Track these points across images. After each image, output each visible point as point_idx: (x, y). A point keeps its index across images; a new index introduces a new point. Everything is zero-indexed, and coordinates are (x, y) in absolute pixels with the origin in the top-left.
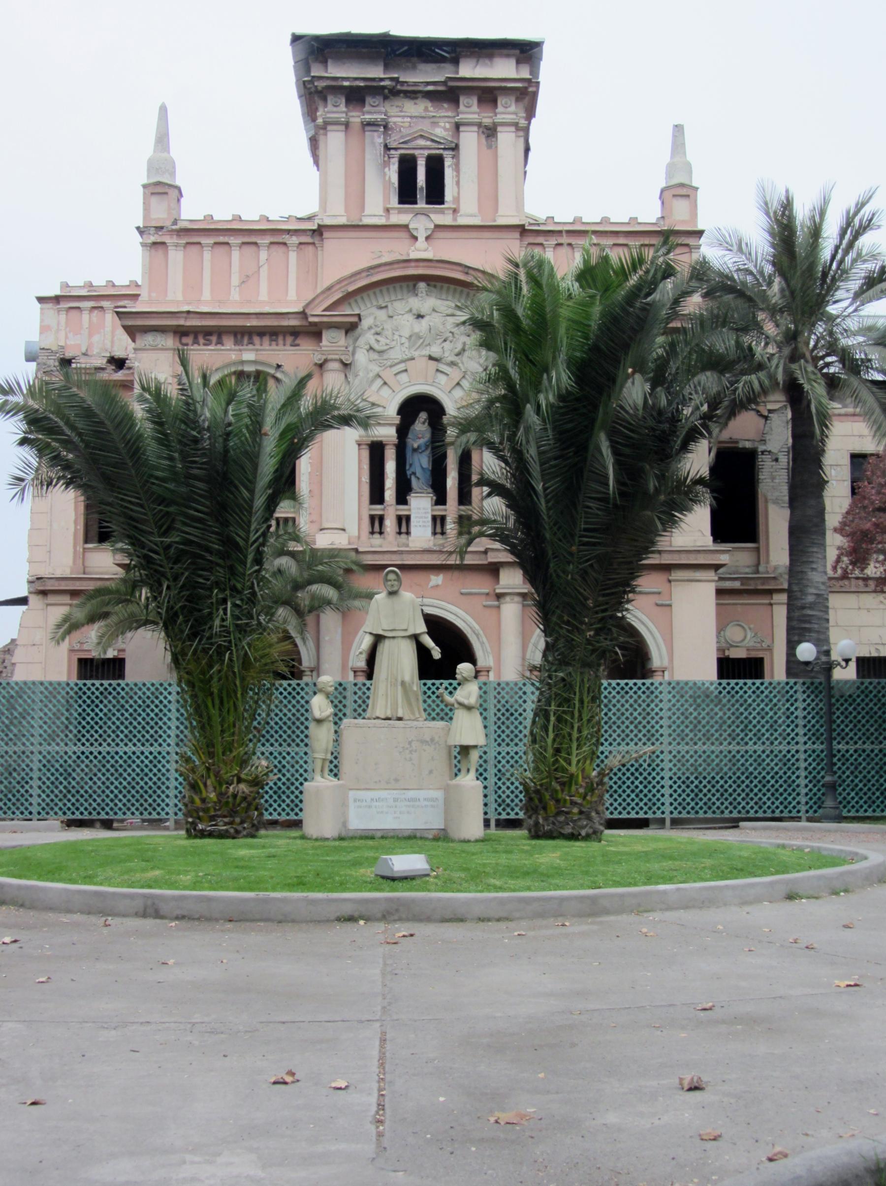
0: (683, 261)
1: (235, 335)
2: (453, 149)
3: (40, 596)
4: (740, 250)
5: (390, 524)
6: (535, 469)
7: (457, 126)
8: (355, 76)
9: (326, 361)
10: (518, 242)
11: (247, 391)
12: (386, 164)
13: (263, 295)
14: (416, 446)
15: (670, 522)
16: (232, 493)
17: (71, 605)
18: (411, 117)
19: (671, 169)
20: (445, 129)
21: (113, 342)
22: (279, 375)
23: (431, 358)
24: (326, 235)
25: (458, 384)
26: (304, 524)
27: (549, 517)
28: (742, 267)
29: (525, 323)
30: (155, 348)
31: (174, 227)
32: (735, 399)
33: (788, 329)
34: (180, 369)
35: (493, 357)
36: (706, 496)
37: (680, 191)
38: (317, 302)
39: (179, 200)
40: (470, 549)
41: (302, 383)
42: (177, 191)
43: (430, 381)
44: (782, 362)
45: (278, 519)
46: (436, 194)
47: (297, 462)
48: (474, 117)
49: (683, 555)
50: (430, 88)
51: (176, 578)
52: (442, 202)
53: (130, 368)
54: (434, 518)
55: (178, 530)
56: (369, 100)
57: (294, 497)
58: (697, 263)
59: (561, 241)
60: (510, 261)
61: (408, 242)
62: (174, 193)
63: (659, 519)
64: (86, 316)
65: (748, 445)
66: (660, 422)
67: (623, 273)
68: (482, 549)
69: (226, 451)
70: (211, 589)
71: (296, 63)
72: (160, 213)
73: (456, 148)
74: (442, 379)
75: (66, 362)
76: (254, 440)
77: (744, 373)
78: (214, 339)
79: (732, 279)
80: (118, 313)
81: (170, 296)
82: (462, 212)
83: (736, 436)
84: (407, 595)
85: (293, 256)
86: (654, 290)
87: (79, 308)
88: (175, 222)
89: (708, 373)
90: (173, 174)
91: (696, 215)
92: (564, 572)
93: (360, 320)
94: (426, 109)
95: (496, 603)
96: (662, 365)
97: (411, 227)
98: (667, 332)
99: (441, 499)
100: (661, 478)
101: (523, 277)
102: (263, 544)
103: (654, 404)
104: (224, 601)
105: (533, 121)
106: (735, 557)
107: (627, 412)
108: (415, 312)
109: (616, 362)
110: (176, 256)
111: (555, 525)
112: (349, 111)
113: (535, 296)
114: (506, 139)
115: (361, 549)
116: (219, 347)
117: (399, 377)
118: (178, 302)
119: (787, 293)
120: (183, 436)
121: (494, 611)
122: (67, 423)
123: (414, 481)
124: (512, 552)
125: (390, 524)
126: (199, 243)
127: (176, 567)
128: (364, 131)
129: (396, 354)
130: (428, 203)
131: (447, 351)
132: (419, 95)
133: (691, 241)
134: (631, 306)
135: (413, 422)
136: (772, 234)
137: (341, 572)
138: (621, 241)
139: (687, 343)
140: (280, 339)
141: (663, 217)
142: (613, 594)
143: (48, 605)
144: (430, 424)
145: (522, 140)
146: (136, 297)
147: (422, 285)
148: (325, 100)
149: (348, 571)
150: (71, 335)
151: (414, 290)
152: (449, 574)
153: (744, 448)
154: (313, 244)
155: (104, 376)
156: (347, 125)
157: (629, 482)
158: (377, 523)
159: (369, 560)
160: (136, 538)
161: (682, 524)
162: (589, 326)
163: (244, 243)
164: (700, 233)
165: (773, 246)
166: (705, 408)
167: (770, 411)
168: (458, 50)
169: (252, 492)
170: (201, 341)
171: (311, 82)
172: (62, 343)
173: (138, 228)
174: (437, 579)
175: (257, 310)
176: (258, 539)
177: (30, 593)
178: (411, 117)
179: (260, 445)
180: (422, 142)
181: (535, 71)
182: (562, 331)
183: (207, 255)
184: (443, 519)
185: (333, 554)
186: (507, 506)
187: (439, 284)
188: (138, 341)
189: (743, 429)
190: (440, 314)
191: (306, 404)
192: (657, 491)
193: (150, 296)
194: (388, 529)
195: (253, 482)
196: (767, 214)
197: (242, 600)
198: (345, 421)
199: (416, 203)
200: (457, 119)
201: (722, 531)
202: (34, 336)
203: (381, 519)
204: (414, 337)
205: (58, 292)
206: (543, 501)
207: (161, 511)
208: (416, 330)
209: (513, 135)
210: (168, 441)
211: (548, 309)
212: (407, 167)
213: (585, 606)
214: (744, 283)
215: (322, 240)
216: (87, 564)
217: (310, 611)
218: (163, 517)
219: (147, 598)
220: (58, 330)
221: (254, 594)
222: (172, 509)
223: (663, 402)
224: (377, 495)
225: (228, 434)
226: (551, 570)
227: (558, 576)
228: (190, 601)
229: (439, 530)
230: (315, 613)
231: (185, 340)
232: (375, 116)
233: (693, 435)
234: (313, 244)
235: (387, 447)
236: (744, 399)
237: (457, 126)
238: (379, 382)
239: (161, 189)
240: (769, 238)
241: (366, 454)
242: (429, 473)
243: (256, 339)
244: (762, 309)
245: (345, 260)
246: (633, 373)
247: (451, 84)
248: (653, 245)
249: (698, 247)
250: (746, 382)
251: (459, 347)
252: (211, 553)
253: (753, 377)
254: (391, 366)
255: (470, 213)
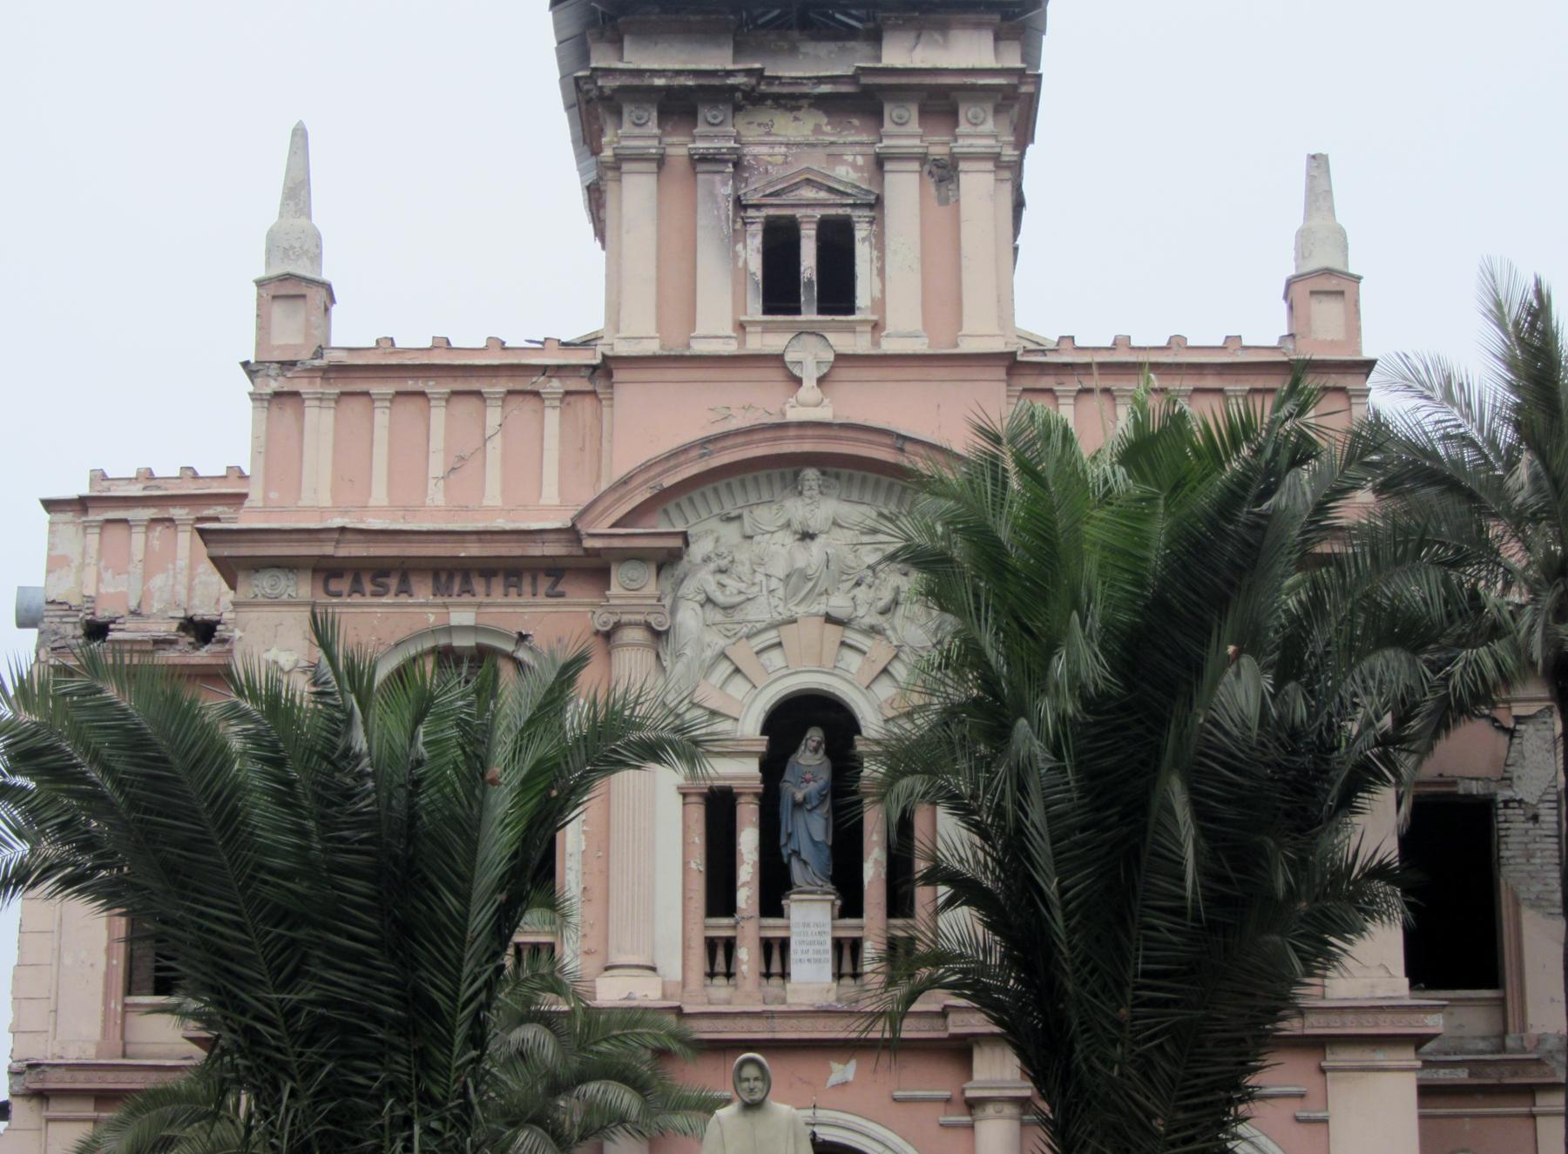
0: (1330, 423)
1: (436, 574)
2: (870, 206)
3: (34, 1103)
4: (1448, 396)
5: (747, 956)
6: (1042, 849)
7: (880, 162)
8: (677, 67)
9: (618, 626)
10: (1003, 386)
11: (456, 695)
12: (738, 236)
13: (493, 495)
14: (799, 796)
15: (1319, 957)
16: (424, 902)
17: (95, 1121)
18: (787, 145)
19: (1304, 240)
20: (854, 166)
21: (190, 589)
22: (522, 655)
23: (829, 619)
24: (619, 375)
25: (885, 671)
26: (572, 956)
27: (1072, 949)
28: (1453, 431)
29: (1015, 557)
30: (274, 602)
31: (317, 363)
32: (1447, 696)
33: (1550, 555)
34: (319, 653)
35: (951, 622)
36: (1393, 899)
37: (1324, 284)
38: (600, 508)
39: (327, 310)
40: (915, 1007)
41: (569, 672)
42: (323, 292)
43: (828, 665)
44: (1540, 621)
45: (518, 947)
46: (837, 292)
47: (559, 835)
48: (912, 144)
49: (1349, 1018)
50: (825, 88)
51: (309, 1072)
52: (851, 310)
53: (224, 641)
54: (838, 944)
55: (314, 977)
56: (705, 113)
57: (551, 902)
58: (1361, 425)
59: (1088, 384)
60: (983, 431)
61: (781, 388)
62: (317, 296)
63: (1297, 949)
64: (138, 537)
65: (1476, 788)
66: (1294, 752)
67: (1213, 455)
68: (937, 1007)
69: (413, 817)
70: (379, 1098)
71: (560, 43)
72: (290, 335)
73: (877, 204)
74: (853, 661)
75: (96, 630)
76: (470, 794)
77: (1463, 643)
78: (393, 582)
79: (1434, 455)
80: (202, 532)
81: (306, 500)
82: (890, 329)
83: (1450, 770)
84: (781, 1110)
85: (552, 417)
86: (1277, 484)
87: (125, 521)
88: (319, 352)
89: (1390, 653)
90: (316, 258)
91: (1359, 329)
92: (1104, 1061)
93: (687, 544)
94: (817, 129)
95: (967, 1119)
96: (1300, 626)
97: (788, 358)
98: (1308, 561)
99: (851, 905)
100: (1300, 865)
101: (1010, 464)
102: (487, 1006)
103: (1281, 716)
104: (407, 1122)
105: (1030, 149)
106: (1455, 1019)
107: (1227, 734)
108: (796, 526)
109: (1203, 633)
110: (320, 421)
111: (1084, 963)
112: (665, 134)
113: (1035, 501)
114: (976, 184)
115: (687, 1009)
116: (403, 599)
117: (765, 656)
118: (322, 511)
119: (1546, 484)
120: (325, 787)
121: (962, 1135)
122: (95, 758)
123: (796, 870)
124: (998, 1022)
125: (747, 956)
126: (367, 394)
127: (309, 1051)
128: (696, 173)
129: (759, 612)
130: (821, 311)
131: (863, 604)
132: (804, 102)
133: (1351, 382)
134: (1230, 522)
135: (794, 749)
136: (1511, 365)
137: (648, 1055)
138: (1210, 382)
139: (1345, 593)
140: (527, 587)
141: (1292, 335)
142: (1205, 1105)
143: (49, 1120)
144: (828, 753)
145: (1007, 188)
146: (239, 498)
147: (811, 474)
148: (618, 113)
149: (662, 1054)
150: (108, 576)
151: (794, 485)
152: (870, 1061)
153: (1469, 796)
154: (594, 393)
155: (171, 656)
156: (661, 161)
157: (1233, 875)
158: (720, 954)
159: (705, 1030)
160: (229, 993)
161: (1346, 960)
162: (1146, 559)
163: (455, 393)
164: (1369, 365)
165: (1514, 389)
166: (1387, 720)
167: (1519, 719)
168: (880, 15)
169: (465, 898)
170: (368, 587)
171: (591, 78)
172: (90, 591)
173: (245, 364)
174: (843, 1071)
175: (480, 526)
176: (476, 994)
177: (13, 1095)
178: (787, 145)
179: (481, 804)
180: (809, 194)
181: (1031, 53)
182: (1091, 566)
183: (382, 417)
184: (856, 945)
185: (632, 1018)
186: (988, 926)
187: (845, 472)
188: (241, 588)
189: (1465, 755)
190: (842, 534)
191: (577, 714)
192: (1292, 895)
193: (266, 497)
194: (744, 968)
195: (467, 880)
196: (1501, 323)
197: (443, 1120)
198: (652, 752)
199: (797, 311)
200: (878, 148)
201: (1425, 967)
202: (35, 576)
203: (730, 945)
204: (796, 579)
205: (84, 490)
206: (1058, 915)
207: (281, 937)
208: (800, 563)
209: (991, 177)
210: (295, 797)
211: (1061, 525)
212: (780, 244)
213: (1150, 1132)
214: (1458, 464)
215: (611, 386)
216: (130, 1037)
217: (582, 1138)
218: (282, 951)
219: (250, 1116)
220: (83, 566)
221: (467, 1107)
222: (301, 934)
223: (1301, 711)
224: (720, 898)
225: (417, 783)
226: (1078, 1056)
227: (1092, 1069)
228: (337, 1123)
229: (847, 967)
230: (592, 1141)
231: (334, 585)
232: (716, 144)
233: (1362, 778)
234: (594, 393)
235: (742, 800)
236: (1466, 696)
237: (880, 162)
238: (725, 668)
239: (293, 289)
240: (1509, 376)
241: (698, 813)
242: (827, 852)
243: (478, 585)
244: (1496, 516)
245: (657, 425)
246: (1238, 654)
247: (864, 80)
248: (1272, 391)
249: (1365, 393)
250: (1468, 662)
251: (887, 596)
252: (380, 1023)
253: (1483, 650)
254: (749, 637)
255: (905, 331)
